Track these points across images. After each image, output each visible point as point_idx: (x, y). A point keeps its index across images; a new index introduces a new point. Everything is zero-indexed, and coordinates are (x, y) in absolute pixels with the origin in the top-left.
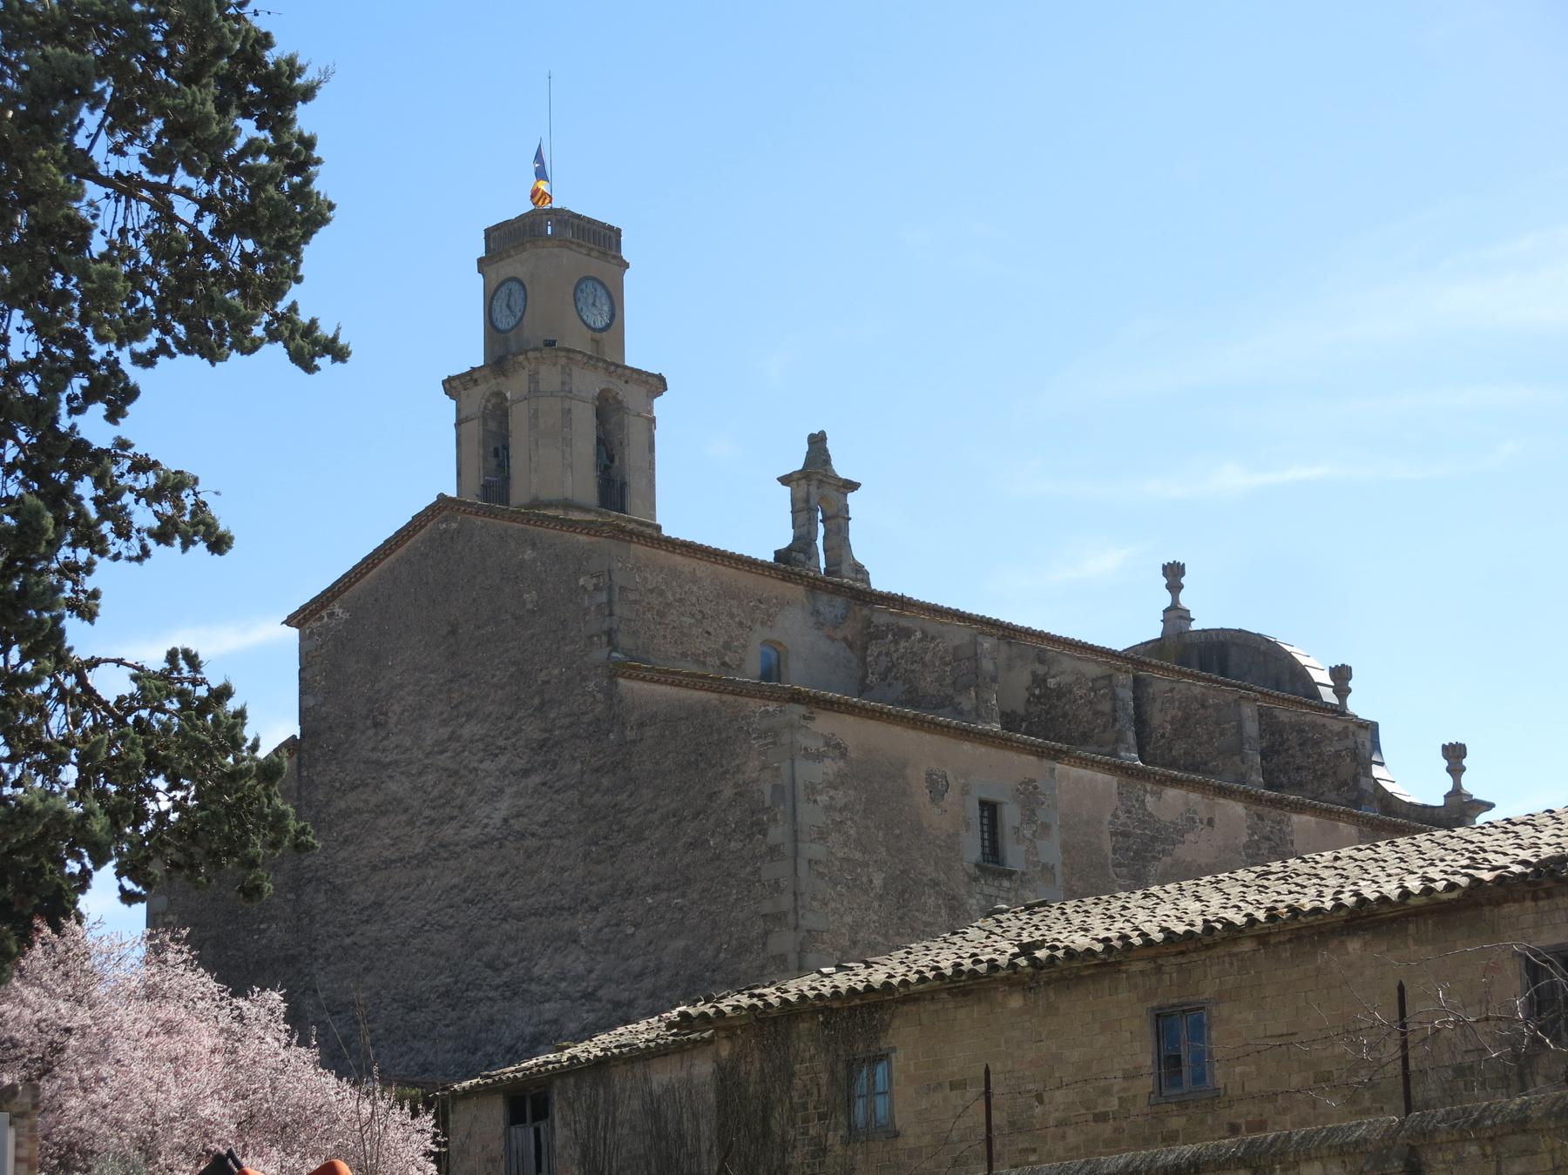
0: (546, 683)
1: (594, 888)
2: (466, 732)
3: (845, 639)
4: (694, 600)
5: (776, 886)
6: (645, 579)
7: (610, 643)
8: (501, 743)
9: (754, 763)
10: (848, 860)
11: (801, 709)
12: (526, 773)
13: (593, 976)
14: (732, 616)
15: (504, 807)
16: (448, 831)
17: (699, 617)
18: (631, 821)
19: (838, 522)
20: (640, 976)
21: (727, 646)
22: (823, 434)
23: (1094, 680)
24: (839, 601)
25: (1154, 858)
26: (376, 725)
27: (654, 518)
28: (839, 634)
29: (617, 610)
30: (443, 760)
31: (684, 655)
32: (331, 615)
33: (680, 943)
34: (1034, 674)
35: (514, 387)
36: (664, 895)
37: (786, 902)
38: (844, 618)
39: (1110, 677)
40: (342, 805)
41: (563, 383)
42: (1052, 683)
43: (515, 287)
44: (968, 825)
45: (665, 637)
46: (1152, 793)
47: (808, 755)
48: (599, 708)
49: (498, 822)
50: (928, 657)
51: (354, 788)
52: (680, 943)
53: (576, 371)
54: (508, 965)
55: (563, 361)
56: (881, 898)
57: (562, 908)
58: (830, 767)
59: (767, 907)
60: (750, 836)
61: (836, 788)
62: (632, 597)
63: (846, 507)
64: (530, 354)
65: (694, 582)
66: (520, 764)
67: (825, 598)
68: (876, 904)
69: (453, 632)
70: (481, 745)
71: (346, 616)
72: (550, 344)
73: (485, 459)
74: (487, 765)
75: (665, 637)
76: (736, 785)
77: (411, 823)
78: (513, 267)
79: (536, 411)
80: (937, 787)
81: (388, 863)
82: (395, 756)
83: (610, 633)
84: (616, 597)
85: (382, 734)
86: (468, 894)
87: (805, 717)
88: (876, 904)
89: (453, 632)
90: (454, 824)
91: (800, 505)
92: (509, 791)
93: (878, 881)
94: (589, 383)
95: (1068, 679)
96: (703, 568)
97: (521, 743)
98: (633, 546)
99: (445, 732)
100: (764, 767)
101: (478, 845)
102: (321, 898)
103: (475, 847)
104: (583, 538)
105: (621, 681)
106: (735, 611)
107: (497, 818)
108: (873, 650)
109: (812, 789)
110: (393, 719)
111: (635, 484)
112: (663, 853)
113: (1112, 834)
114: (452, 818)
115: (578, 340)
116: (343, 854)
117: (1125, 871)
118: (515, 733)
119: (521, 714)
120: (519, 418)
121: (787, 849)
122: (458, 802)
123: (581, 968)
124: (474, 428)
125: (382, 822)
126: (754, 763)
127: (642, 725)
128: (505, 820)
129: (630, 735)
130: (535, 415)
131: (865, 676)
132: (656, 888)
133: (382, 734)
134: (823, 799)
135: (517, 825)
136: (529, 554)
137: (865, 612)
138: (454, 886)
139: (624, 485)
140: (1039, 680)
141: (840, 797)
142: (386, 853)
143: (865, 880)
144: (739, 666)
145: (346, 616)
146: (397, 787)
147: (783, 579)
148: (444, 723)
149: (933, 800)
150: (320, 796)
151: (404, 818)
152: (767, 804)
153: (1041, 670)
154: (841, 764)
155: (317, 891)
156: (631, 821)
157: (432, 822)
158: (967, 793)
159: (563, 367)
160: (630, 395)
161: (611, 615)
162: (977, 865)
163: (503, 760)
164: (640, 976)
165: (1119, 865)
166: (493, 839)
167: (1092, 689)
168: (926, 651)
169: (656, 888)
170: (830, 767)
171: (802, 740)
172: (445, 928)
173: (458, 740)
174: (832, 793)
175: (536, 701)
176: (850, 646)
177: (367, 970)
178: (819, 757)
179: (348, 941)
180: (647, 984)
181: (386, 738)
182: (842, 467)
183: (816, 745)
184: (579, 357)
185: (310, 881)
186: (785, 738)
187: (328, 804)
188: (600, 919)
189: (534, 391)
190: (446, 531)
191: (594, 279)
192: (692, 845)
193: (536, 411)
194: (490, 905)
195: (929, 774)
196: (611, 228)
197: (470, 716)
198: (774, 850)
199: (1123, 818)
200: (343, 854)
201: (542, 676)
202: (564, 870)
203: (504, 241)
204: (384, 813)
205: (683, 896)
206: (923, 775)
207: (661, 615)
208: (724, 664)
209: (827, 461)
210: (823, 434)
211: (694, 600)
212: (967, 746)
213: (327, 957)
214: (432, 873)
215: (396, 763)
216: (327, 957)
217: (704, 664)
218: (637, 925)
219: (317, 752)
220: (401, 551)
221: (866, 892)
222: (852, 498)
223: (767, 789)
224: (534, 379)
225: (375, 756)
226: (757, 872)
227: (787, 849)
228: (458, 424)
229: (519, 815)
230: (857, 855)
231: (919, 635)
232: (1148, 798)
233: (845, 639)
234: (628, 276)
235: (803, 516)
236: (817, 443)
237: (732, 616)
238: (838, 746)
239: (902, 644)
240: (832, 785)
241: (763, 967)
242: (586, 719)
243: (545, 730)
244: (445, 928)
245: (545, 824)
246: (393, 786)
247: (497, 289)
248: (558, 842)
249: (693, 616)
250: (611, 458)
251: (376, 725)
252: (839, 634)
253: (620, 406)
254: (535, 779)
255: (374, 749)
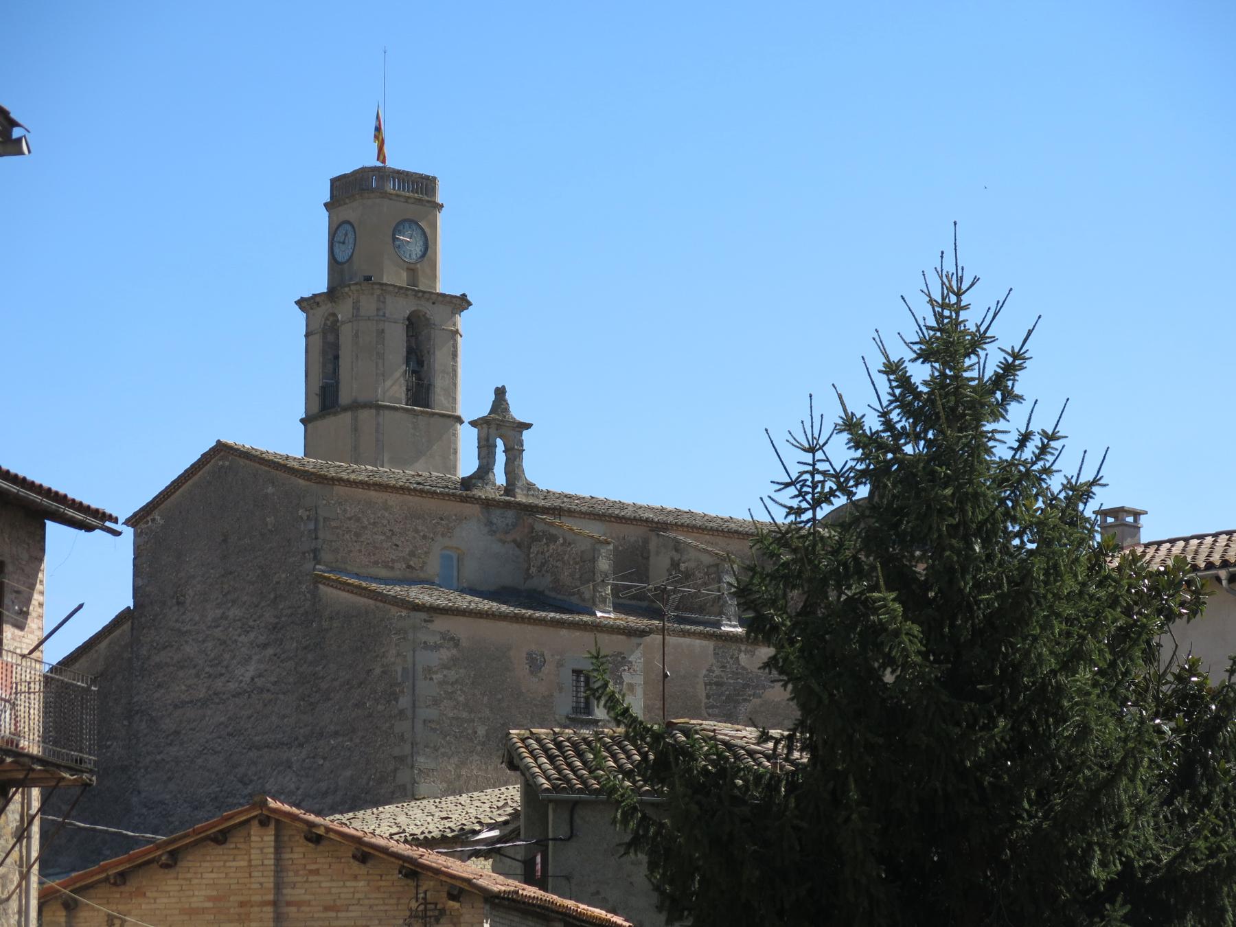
0: (278, 583)
1: (302, 731)
2: (231, 614)
3: (514, 541)
4: (385, 522)
5: (402, 738)
6: (345, 511)
7: (315, 558)
8: (251, 623)
9: (393, 652)
10: (457, 719)
11: (423, 615)
12: (265, 646)
13: (299, 792)
14: (416, 531)
15: (251, 670)
16: (219, 683)
17: (389, 534)
18: (324, 686)
19: (514, 454)
20: (325, 794)
21: (412, 554)
22: (504, 387)
23: (708, 567)
24: (510, 514)
25: (745, 700)
26: (178, 603)
27: (454, 409)
28: (509, 538)
29: (321, 535)
30: (217, 632)
31: (376, 563)
32: (153, 520)
33: (348, 773)
34: (672, 559)
35: (344, 311)
36: (340, 739)
37: (407, 749)
38: (514, 525)
39: (717, 565)
40: (157, 659)
41: (378, 310)
42: (683, 566)
43: (348, 227)
44: (561, 689)
45: (360, 551)
46: (746, 652)
47: (426, 646)
48: (308, 603)
49: (248, 680)
50: (566, 557)
51: (165, 648)
52: (348, 773)
53: (389, 299)
54: (251, 781)
55: (379, 292)
56: (483, 744)
57: (283, 744)
58: (445, 654)
59: (397, 751)
60: (389, 702)
61: (449, 669)
62: (334, 524)
63: (521, 443)
64: (353, 288)
65: (386, 509)
66: (262, 639)
67: (498, 512)
68: (479, 748)
69: (225, 541)
70: (239, 624)
71: (162, 522)
72: (368, 279)
73: (324, 365)
74: (243, 638)
75: (360, 551)
76: (383, 666)
77: (197, 676)
78: (349, 212)
79: (357, 331)
80: (535, 663)
81: (184, 703)
82: (188, 627)
83: (315, 551)
84: (321, 524)
85: (182, 610)
86: (230, 729)
87: (425, 621)
88: (479, 748)
89: (225, 541)
90: (223, 679)
91: (483, 443)
92: (255, 658)
93: (481, 731)
94: (401, 308)
95: (692, 565)
96: (393, 499)
97: (263, 625)
98: (336, 488)
99: (219, 612)
100: (398, 655)
101: (236, 695)
102: (144, 725)
103: (234, 696)
104: (301, 481)
105: (321, 586)
106: (420, 528)
107: (249, 675)
108: (534, 549)
109: (429, 670)
110: (188, 601)
111: (439, 383)
112: (340, 709)
113: (706, 684)
114: (222, 675)
115: (394, 276)
116: (157, 695)
117: (717, 711)
118: (260, 617)
119: (263, 604)
120: (346, 332)
121: (409, 713)
122: (225, 663)
123: (293, 786)
124: (317, 339)
125: (181, 674)
126: (393, 652)
127: (331, 618)
128: (252, 679)
129: (325, 624)
130: (356, 335)
131: (528, 569)
132: (336, 734)
133: (182, 610)
134: (438, 677)
135: (259, 682)
136: (270, 490)
137: (530, 521)
138: (221, 723)
139: (430, 385)
140: (675, 565)
141: (452, 675)
142: (183, 696)
143: (470, 731)
144: (422, 568)
145: (162, 522)
146: (190, 649)
147: (462, 501)
148: (219, 606)
149: (532, 672)
150: (144, 652)
151: (193, 671)
152: (399, 680)
153: (677, 557)
154: (454, 651)
155: (141, 721)
156: (324, 686)
157: (210, 676)
158: (562, 665)
159: (379, 296)
160: (435, 313)
161: (316, 538)
162: (567, 717)
163: (252, 635)
164: (325, 794)
165: (712, 707)
166: (245, 691)
167: (706, 574)
168: (565, 552)
169: (336, 734)
170: (445, 654)
171: (422, 636)
172: (216, 753)
173: (226, 618)
174: (445, 672)
175: (272, 596)
176: (519, 545)
177: (170, 779)
178: (436, 647)
179: (159, 757)
180: (329, 800)
181: (184, 613)
182: (518, 412)
183: (432, 640)
184: (391, 288)
185: (137, 712)
186: (410, 636)
187: (149, 658)
188: (304, 752)
189: (356, 316)
190: (222, 466)
191: (404, 221)
192: (356, 705)
193: (357, 331)
194: (242, 738)
195: (529, 654)
196: (427, 178)
197: (234, 602)
198: (402, 712)
199: (717, 672)
200: (157, 695)
201: (275, 579)
202: (284, 716)
203: (347, 189)
204: (182, 668)
205: (351, 740)
206: (524, 655)
207: (357, 535)
208: (409, 567)
209: (506, 410)
210: (504, 387)
211: (385, 522)
212: (564, 632)
213: (146, 768)
214: (209, 712)
215: (188, 632)
216: (146, 768)
217: (392, 568)
218: (325, 759)
219: (143, 620)
220: (196, 478)
221: (471, 740)
222: (526, 435)
223: (399, 669)
224: (356, 306)
225: (178, 625)
226: (392, 727)
227: (409, 713)
228: (307, 336)
229: (260, 676)
230: (465, 715)
231: (561, 540)
232: (742, 656)
233: (514, 541)
234: (441, 218)
235: (485, 451)
236: (500, 393)
237: (416, 531)
238: (452, 639)
239: (552, 546)
240: (445, 667)
241: (393, 793)
242: (301, 611)
243: (276, 617)
244: (216, 753)
245: (275, 683)
246: (187, 649)
247: (337, 228)
248: (281, 697)
249: (384, 534)
250: (420, 363)
251: (178, 603)
252: (509, 538)
253: (428, 323)
254: (270, 651)
255: (177, 621)
